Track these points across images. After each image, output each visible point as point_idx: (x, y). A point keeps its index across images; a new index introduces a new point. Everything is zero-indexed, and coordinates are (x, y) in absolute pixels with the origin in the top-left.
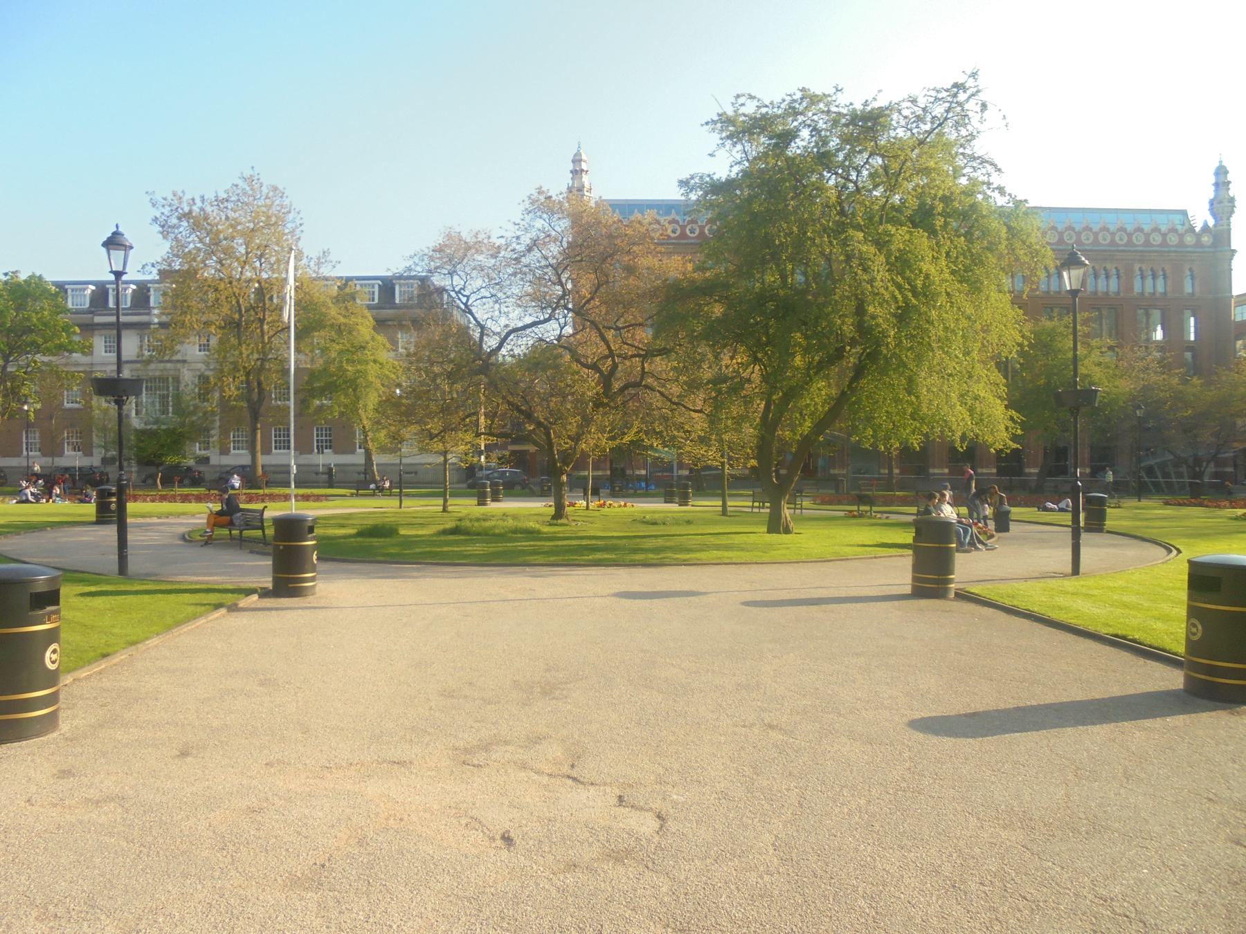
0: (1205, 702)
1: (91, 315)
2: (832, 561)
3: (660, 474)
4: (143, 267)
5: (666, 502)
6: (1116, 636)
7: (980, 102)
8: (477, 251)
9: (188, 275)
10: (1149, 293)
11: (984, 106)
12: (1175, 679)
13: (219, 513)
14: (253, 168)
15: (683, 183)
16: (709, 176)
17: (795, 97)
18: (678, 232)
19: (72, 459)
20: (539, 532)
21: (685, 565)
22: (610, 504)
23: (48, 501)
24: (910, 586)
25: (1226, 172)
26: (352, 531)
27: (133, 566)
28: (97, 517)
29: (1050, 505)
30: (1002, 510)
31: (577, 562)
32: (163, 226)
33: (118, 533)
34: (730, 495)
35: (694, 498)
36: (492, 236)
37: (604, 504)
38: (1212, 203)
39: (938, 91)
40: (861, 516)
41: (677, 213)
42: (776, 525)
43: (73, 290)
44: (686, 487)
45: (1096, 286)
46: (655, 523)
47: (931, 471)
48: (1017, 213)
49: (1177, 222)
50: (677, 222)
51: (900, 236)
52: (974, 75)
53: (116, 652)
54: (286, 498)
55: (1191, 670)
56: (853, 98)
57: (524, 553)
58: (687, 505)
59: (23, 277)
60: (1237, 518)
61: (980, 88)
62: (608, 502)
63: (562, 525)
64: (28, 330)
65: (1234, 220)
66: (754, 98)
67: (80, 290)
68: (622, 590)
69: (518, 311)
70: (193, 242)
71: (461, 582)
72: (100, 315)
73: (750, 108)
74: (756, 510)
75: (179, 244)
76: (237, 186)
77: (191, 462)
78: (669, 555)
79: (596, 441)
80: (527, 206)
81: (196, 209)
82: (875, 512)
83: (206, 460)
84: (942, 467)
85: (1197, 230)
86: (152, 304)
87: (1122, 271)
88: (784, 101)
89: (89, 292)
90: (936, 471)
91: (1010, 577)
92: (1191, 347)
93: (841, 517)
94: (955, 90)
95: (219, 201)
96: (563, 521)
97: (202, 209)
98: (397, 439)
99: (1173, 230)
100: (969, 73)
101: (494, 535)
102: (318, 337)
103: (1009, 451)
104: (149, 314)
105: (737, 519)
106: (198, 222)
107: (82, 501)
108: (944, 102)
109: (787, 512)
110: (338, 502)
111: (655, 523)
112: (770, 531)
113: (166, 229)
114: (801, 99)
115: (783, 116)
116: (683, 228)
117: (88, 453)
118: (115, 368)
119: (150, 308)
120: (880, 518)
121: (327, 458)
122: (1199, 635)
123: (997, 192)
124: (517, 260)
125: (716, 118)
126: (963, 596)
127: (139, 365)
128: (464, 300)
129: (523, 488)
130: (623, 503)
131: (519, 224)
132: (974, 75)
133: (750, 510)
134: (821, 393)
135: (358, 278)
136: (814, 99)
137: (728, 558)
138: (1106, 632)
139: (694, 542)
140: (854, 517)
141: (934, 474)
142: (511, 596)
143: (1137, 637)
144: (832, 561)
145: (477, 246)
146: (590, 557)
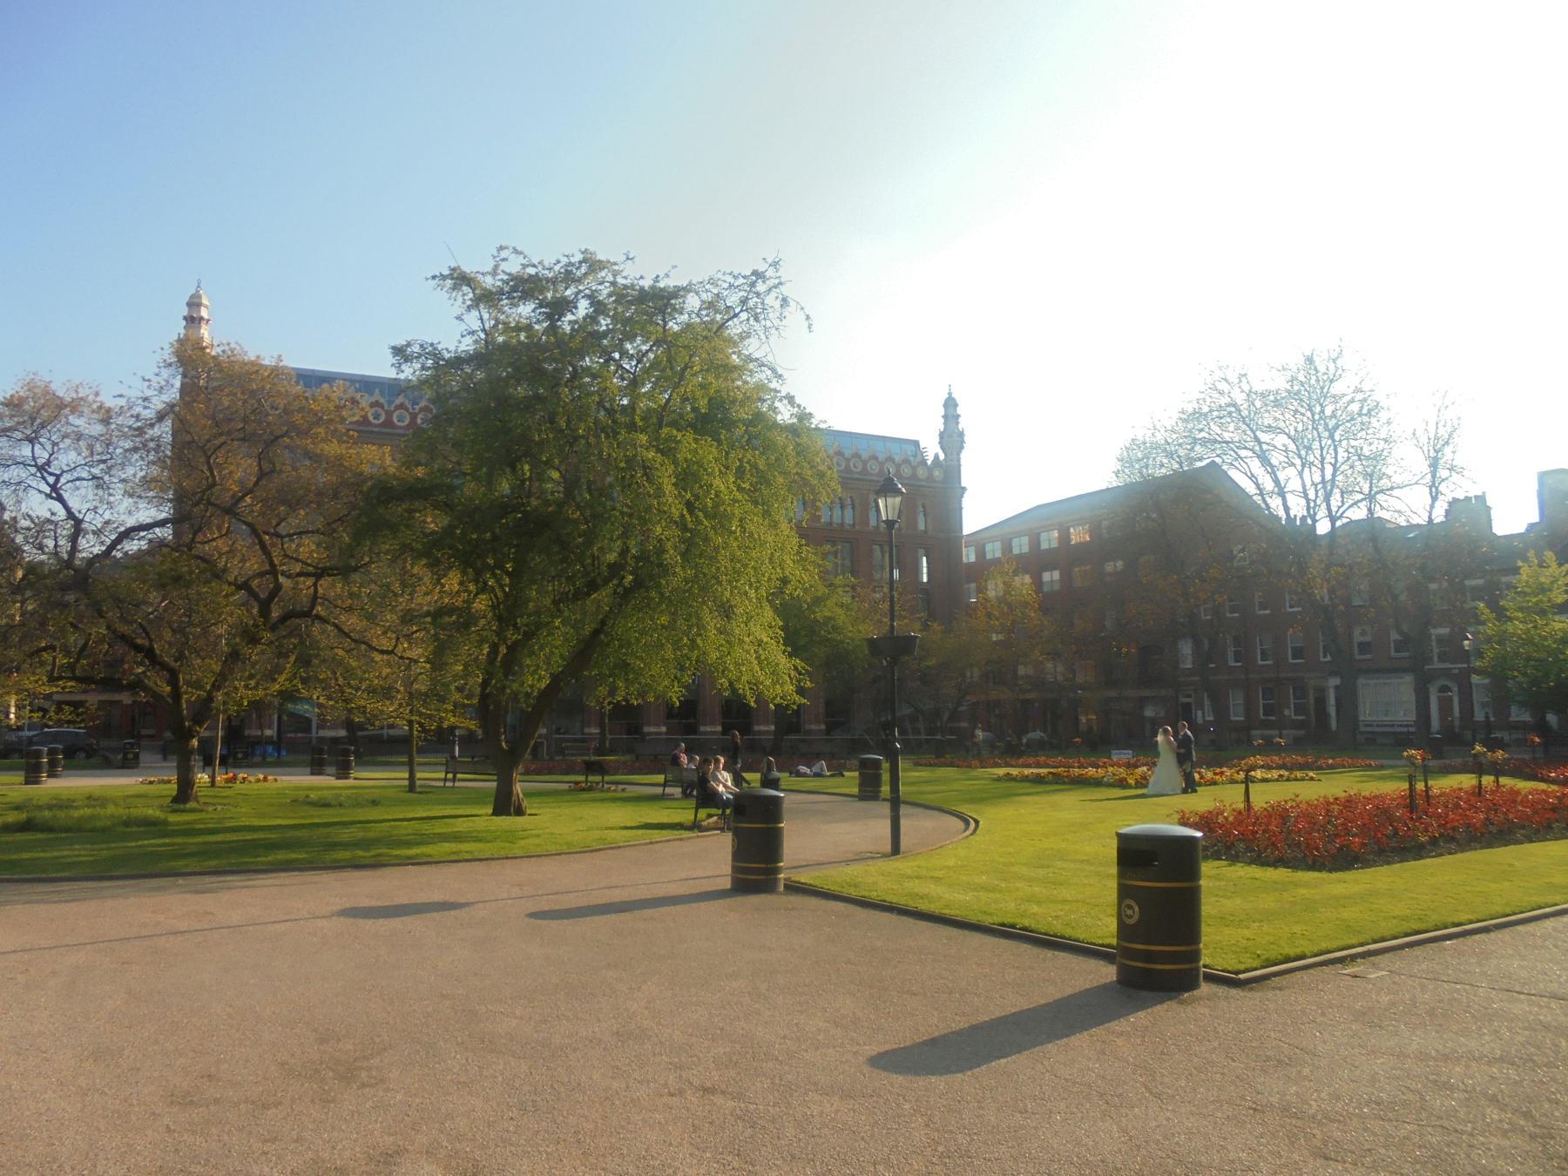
0: (1144, 994)
2: (600, 850)
3: (292, 735)
5: (312, 774)
6: (1003, 925)
7: (781, 297)
8: (73, 412)
10: (849, 525)
11: (785, 302)
12: (1108, 973)
15: (400, 352)
16: (432, 345)
17: (573, 260)
18: (382, 419)
20: (165, 823)
21: (413, 864)
22: (244, 778)
24: (730, 878)
25: (956, 405)
29: (803, 769)
30: (770, 777)
31: (253, 867)
33: (697, 894)
34: (420, 764)
35: (358, 768)
36: (102, 393)
37: (234, 778)
38: (942, 435)
39: (735, 277)
40: (590, 789)
41: (382, 394)
42: (505, 804)
44: (346, 753)
45: (843, 517)
46: (327, 805)
47: (646, 729)
48: (801, 428)
49: (910, 453)
50: (382, 406)
51: (687, 443)
52: (775, 264)
56: (642, 273)
58: (347, 778)
60: (999, 779)
61: (783, 280)
62: (241, 776)
63: (193, 811)
65: (963, 455)
66: (521, 253)
68: (348, 906)
69: (128, 502)
73: (513, 266)
74: (449, 784)
78: (384, 851)
80: (166, 357)
82: (607, 783)
84: (658, 725)
85: (929, 462)
87: (857, 501)
88: (558, 262)
90: (652, 729)
91: (826, 860)
92: (925, 590)
93: (565, 790)
94: (754, 278)
96: (191, 805)
99: (906, 461)
100: (770, 261)
101: (93, 830)
103: (795, 707)
105: (430, 796)
108: (740, 290)
111: (327, 805)
112: (497, 812)
114: (580, 262)
115: (554, 281)
116: (389, 414)
120: (615, 791)
122: (1136, 917)
123: (786, 402)
124: (140, 431)
125: (446, 272)
126: (795, 888)
128: (51, 480)
129: (89, 756)
130: (261, 777)
131: (149, 380)
132: (775, 264)
133: (441, 784)
136: (594, 265)
137: (467, 852)
138: (991, 921)
139: (404, 832)
140: (583, 790)
141: (650, 734)
142: (184, 926)
143: (1027, 925)
144: (600, 850)
145: (75, 406)
146: (270, 858)
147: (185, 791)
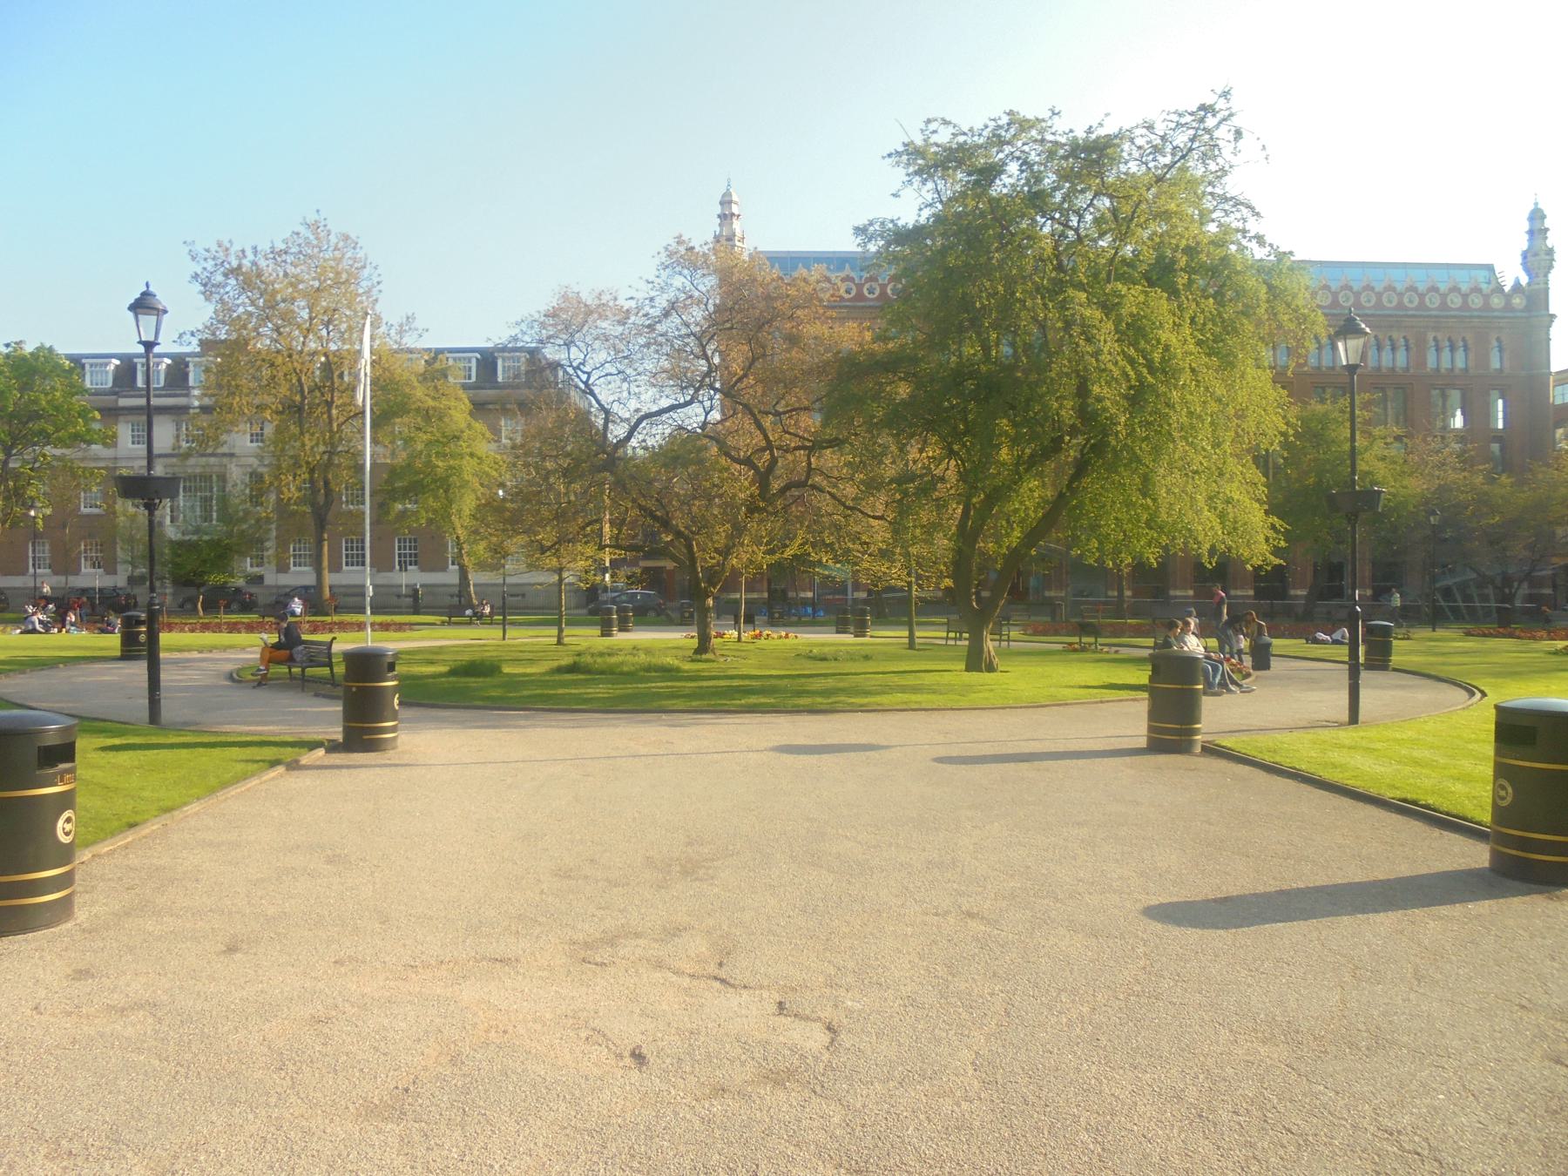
1: (114, 397)
2: (1047, 706)
3: (830, 597)
4: (181, 336)
5: (838, 632)
6: (1405, 800)
7: (1233, 129)
8: (600, 316)
9: (237, 346)
11: (1238, 134)
12: (1478, 856)
13: (276, 646)
14: (318, 211)
15: (860, 231)
16: (892, 221)
17: (1000, 123)
18: (853, 293)
19: (91, 577)
20: (678, 670)
21: (862, 711)
22: (768, 635)
23: (60, 631)
24: (1145, 738)
25: (1543, 217)
26: (443, 669)
27: (167, 712)
28: (122, 651)
29: (1321, 636)
30: (1261, 642)
31: (726, 708)
32: (205, 285)
33: (149, 671)
34: (919, 624)
35: (873, 627)
36: (619, 297)
37: (760, 634)
38: (1525, 255)
39: (1180, 115)
40: (1083, 650)
41: (852, 269)
42: (977, 661)
43: (91, 365)
44: (864, 613)
45: (1379, 361)
46: (824, 659)
47: (1172, 593)
48: (1280, 268)
49: (1481, 279)
50: (852, 280)
51: (1132, 297)
52: (1225, 94)
53: (145, 821)
54: (361, 627)
55: (1498, 844)
56: (1073, 124)
57: (660, 696)
58: (864, 636)
59: (29, 348)
60: (1556, 653)
61: (1233, 111)
62: (765, 633)
63: (707, 661)
64: (36, 416)
65: (1553, 277)
66: (949, 123)
67: (101, 365)
68: (783, 743)
69: (652, 391)
70: (243, 305)
71: (580, 732)
72: (126, 397)
73: (943, 136)
74: (951, 642)
75: (225, 308)
76: (298, 234)
77: (241, 582)
78: (842, 698)
79: (750, 555)
80: (664, 260)
81: (246, 263)
82: (1101, 645)
83: (259, 579)
84: (1185, 588)
85: (1507, 289)
86: (191, 383)
87: (1412, 341)
88: (986, 127)
89: (112, 367)
90: (1178, 593)
91: (1271, 726)
92: (1498, 437)
93: (1058, 651)
94: (1202, 113)
95: (276, 254)
96: (709, 656)
97: (254, 263)
98: (499, 552)
99: (1476, 290)
100: (1219, 93)
101: (622, 673)
102: (400, 425)
103: (1269, 568)
104: (187, 395)
105: (927, 653)
106: (249, 279)
107: (103, 631)
108: (1188, 128)
109: (990, 645)
110: (425, 632)
111: (824, 659)
112: (969, 668)
113: (209, 289)
114: (1008, 124)
115: (985, 147)
116: (860, 287)
117: (111, 570)
118: (145, 463)
119: (188, 388)
120: (1107, 652)
121: (412, 577)
122: (1509, 799)
123: (1254, 241)
124: (651, 327)
125: (901, 149)
126: (1212, 751)
127: (174, 460)
128: (584, 377)
129: (658, 615)
130: (783, 634)
131: (653, 282)
132: (1225, 94)
133: (943, 642)
134: (1033, 494)
135: (451, 351)
136: (1024, 125)
137: (916, 702)
138: (1392, 796)
139: (873, 683)
140: (1075, 650)
141: (1176, 597)
142: (643, 751)
143: (1431, 802)
144: (1047, 706)
145: (600, 310)
146: (743, 702)
147: (703, 646)
